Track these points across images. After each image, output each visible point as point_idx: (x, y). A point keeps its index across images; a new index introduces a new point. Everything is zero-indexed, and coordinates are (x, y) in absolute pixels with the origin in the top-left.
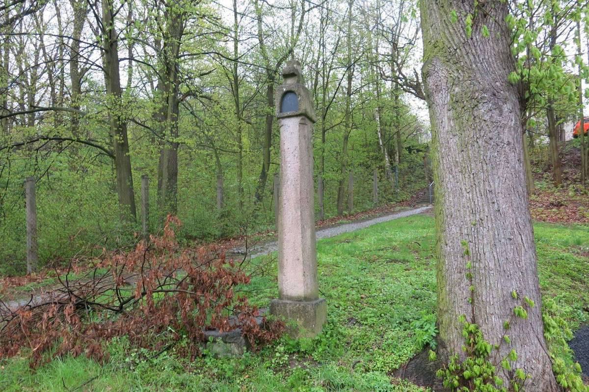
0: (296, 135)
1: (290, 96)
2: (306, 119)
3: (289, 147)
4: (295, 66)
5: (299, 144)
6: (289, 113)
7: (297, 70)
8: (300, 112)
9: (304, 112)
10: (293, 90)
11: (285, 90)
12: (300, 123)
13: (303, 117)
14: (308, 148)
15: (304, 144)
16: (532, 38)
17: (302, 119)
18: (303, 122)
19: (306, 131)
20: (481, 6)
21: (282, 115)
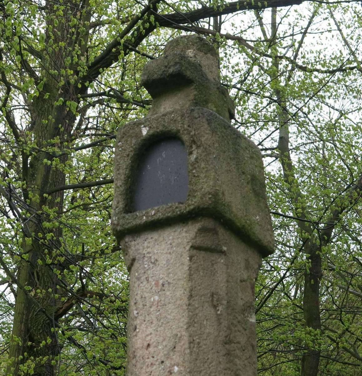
0: (178, 293)
1: (164, 156)
2: (221, 231)
3: (153, 339)
4: (190, 53)
5: (190, 325)
6: (153, 213)
7: (197, 67)
8: (193, 203)
9: (207, 201)
10: (173, 127)
11: (145, 131)
12: (193, 247)
13: (209, 223)
14: (228, 341)
15: (210, 328)
16: (49, 341)
17: (202, 231)
18: (207, 241)
19: (221, 277)
20: (171, 373)
21: (132, 220)
